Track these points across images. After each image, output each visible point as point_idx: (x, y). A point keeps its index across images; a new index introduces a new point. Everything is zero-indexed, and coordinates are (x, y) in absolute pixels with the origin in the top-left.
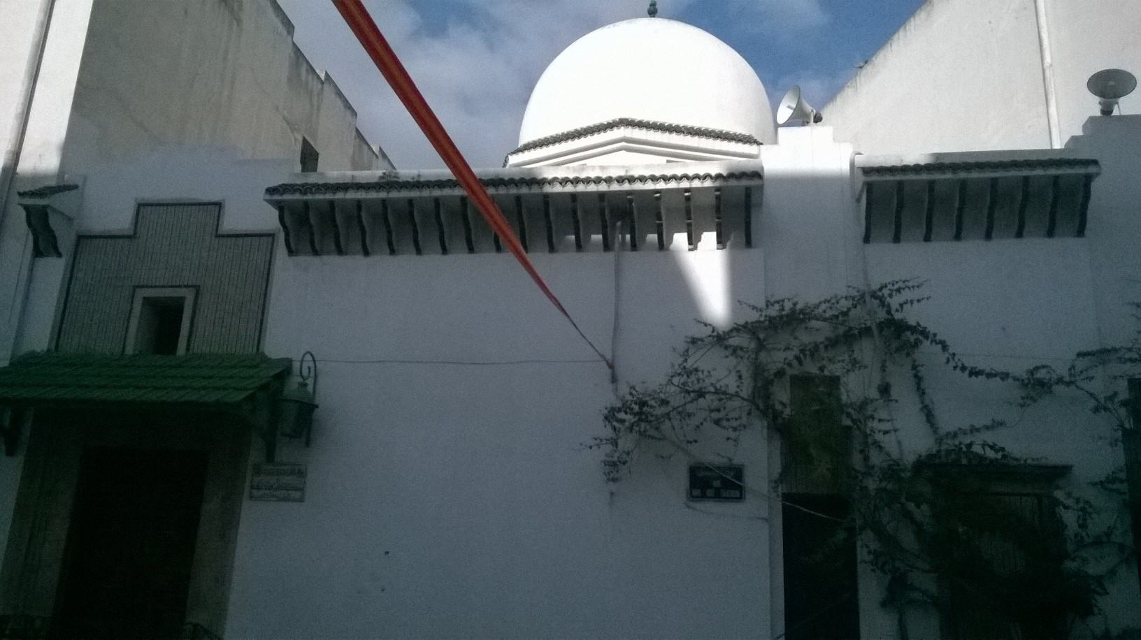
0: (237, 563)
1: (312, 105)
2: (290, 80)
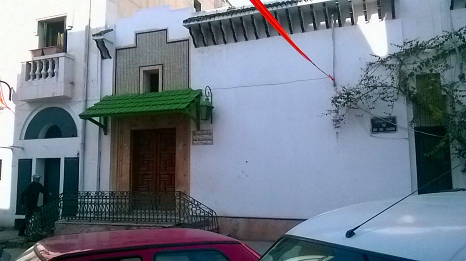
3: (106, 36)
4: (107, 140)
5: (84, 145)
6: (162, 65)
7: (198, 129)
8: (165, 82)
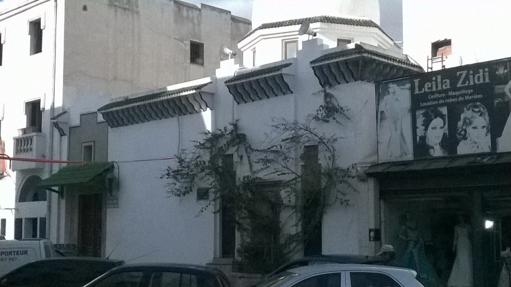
0: (107, 231)
1: (194, 24)
2: (176, 21)
3: (60, 119)
4: (63, 202)
5: (49, 207)
6: (94, 141)
7: (111, 196)
8: (96, 157)
